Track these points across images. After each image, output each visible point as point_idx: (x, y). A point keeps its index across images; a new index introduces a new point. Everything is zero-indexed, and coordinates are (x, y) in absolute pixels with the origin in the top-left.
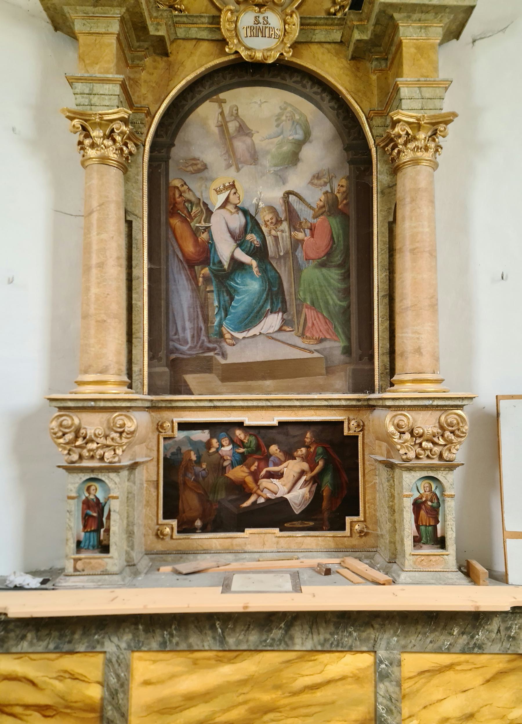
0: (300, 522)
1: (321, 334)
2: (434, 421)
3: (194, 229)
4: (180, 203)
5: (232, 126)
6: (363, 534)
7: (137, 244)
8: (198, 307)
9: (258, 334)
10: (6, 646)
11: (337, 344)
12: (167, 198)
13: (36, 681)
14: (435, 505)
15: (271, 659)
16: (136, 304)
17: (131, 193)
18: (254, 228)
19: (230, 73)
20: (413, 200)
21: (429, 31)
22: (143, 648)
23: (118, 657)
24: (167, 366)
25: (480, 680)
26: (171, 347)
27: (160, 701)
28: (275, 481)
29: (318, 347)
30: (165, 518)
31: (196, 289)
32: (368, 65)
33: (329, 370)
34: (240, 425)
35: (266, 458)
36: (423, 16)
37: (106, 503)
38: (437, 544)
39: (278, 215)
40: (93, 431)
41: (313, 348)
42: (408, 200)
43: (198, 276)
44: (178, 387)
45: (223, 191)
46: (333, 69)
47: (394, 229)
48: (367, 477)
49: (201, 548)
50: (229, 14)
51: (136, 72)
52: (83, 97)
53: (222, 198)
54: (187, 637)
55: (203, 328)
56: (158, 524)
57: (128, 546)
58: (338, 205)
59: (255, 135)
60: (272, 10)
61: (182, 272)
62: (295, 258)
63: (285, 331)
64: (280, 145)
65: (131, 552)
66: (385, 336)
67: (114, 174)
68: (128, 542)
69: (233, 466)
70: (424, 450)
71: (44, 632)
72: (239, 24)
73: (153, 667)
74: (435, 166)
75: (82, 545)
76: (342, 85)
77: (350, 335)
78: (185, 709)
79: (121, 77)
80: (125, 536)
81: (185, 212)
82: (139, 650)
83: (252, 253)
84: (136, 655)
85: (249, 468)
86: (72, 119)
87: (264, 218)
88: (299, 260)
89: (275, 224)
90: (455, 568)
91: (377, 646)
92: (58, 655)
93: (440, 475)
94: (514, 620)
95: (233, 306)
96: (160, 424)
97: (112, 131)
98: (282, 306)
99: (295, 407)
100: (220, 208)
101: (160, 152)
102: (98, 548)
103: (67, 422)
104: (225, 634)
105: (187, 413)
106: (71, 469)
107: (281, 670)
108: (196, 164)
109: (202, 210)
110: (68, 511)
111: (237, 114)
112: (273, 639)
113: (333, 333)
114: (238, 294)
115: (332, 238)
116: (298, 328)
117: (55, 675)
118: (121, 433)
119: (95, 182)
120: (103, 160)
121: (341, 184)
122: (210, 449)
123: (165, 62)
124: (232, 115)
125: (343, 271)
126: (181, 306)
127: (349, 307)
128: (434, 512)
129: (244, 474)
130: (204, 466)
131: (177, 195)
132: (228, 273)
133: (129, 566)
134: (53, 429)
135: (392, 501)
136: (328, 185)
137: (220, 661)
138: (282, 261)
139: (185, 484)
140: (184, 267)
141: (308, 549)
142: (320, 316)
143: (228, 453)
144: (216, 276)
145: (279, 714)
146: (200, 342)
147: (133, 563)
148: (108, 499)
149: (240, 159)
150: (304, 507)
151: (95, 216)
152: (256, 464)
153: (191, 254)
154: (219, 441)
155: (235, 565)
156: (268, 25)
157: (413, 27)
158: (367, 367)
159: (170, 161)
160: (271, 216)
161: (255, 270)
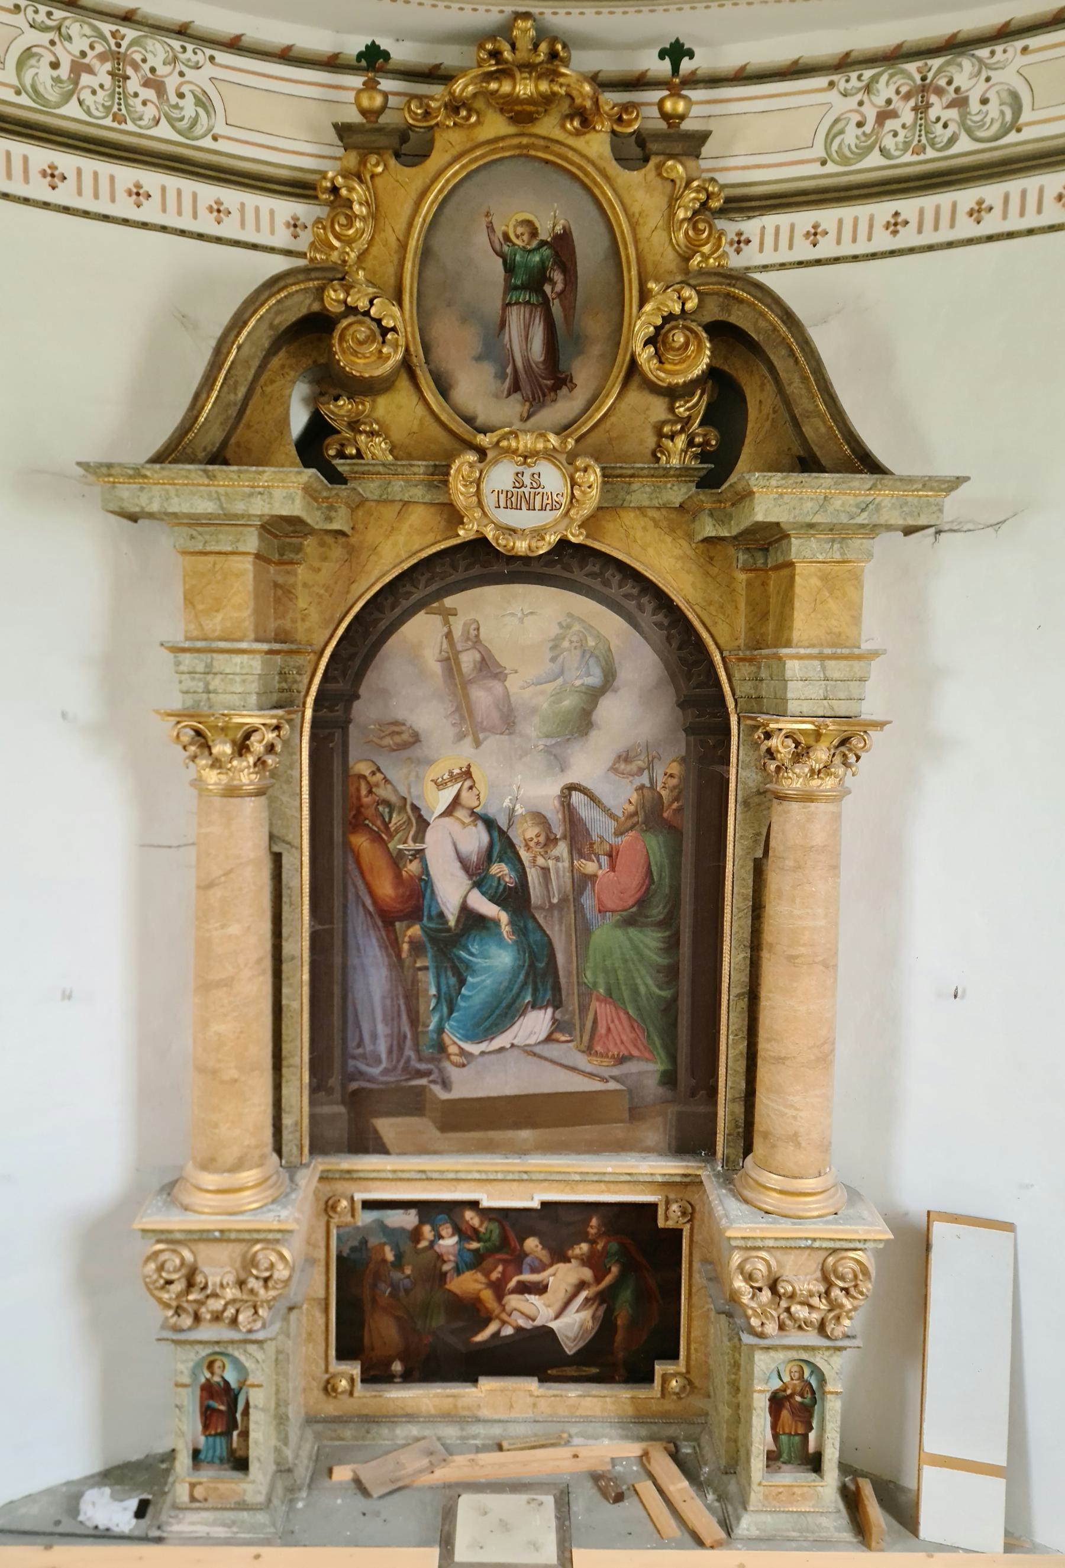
0: (575, 1367)
1: (622, 1048)
2: (814, 1266)
3: (394, 855)
4: (368, 807)
5: (468, 660)
7: (290, 896)
8: (401, 997)
9: (508, 1046)
14: (807, 1401)
16: (288, 1006)
17: (279, 803)
18: (505, 853)
19: (464, 558)
21: (848, 547)
24: (343, 1103)
26: (350, 1069)
28: (533, 1298)
29: (616, 1071)
31: (397, 963)
33: (636, 1114)
34: (474, 1205)
35: (518, 1261)
37: (241, 1389)
38: (807, 1464)
39: (550, 828)
40: (218, 1280)
41: (606, 1072)
42: (790, 863)
43: (400, 940)
44: (364, 1142)
45: (449, 784)
46: (664, 560)
47: (764, 868)
48: (695, 1299)
49: (402, 1412)
50: (466, 468)
51: (288, 572)
52: (193, 679)
53: (446, 796)
55: (409, 1036)
57: (279, 1440)
58: (662, 810)
59: (510, 677)
61: (372, 932)
62: (579, 909)
63: (557, 1041)
64: (558, 696)
65: (284, 1448)
66: (738, 1069)
68: (279, 1432)
69: (458, 1271)
72: (483, 486)
75: (202, 1456)
77: (676, 1050)
81: (379, 823)
85: (487, 1275)
87: (524, 833)
88: (587, 912)
89: (545, 845)
93: (819, 1361)
95: (464, 996)
96: (330, 1202)
98: (554, 995)
100: (443, 815)
101: (332, 711)
102: (229, 1461)
108: (399, 733)
109: (409, 819)
110: (177, 1406)
111: (477, 636)
113: (645, 1047)
115: (649, 872)
116: (581, 1037)
118: (266, 1280)
121: (669, 772)
122: (418, 1242)
123: (343, 547)
124: (468, 639)
125: (667, 934)
126: (369, 992)
127: (675, 999)
131: (364, 792)
132: (457, 934)
133: (281, 1471)
134: (150, 1277)
135: (735, 1374)
136: (646, 772)
138: (556, 913)
139: (374, 1301)
140: (375, 925)
141: (587, 1416)
142: (622, 1015)
143: (451, 1250)
144: (433, 940)
146: (403, 1061)
147: (287, 1467)
149: (482, 723)
150: (582, 1344)
152: (500, 1268)
153: (388, 900)
156: (539, 490)
157: (819, 540)
158: (702, 1109)
159: (352, 728)
160: (536, 830)
161: (505, 929)
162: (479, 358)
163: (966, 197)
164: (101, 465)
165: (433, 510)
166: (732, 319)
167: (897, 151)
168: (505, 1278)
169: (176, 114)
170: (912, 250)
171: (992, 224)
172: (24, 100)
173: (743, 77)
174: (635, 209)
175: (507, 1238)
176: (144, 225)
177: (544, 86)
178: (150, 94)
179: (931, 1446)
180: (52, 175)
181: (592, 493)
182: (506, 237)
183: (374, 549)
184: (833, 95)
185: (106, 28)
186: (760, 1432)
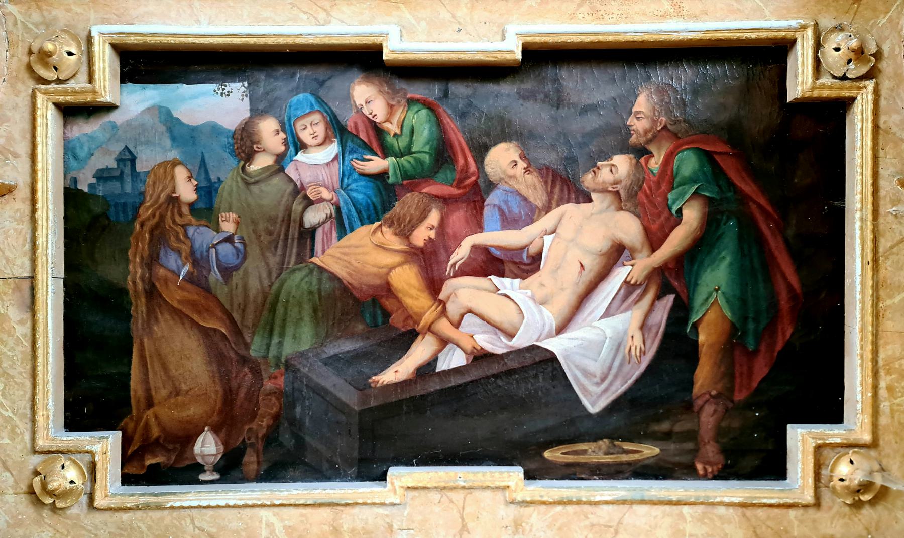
28: (506, 284)
30: (73, 423)
35: (474, 196)
85: (405, 234)
122: (249, 157)
129: (388, 259)
139: (152, 293)
150: (619, 388)
152: (434, 217)
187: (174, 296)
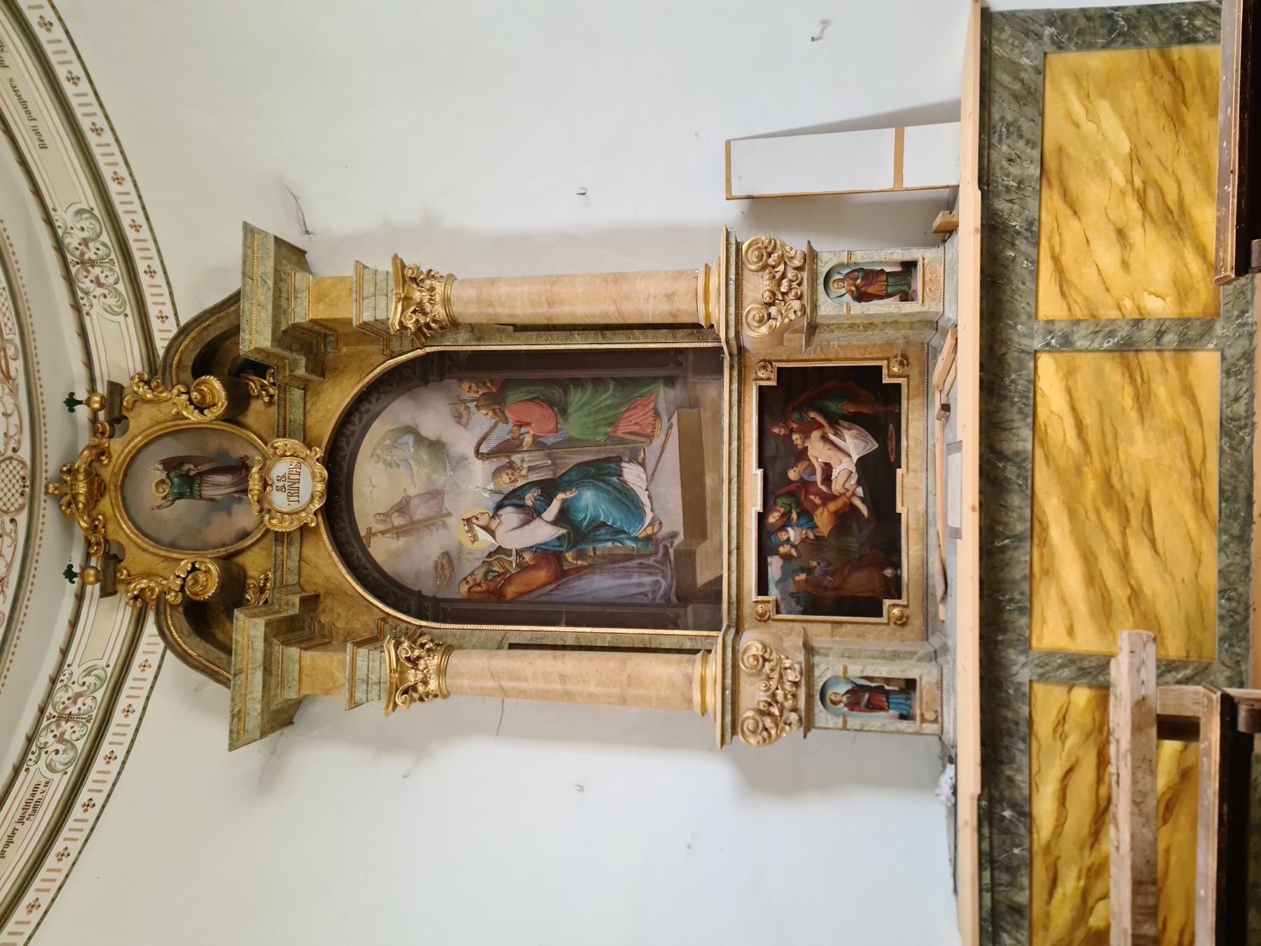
5: (398, 521)
6: (904, 361)
10: (1021, 802)
11: (662, 394)
12: (482, 602)
13: (1067, 768)
14: (860, 275)
15: (1044, 480)
20: (491, 305)
22: (1027, 635)
23: (1037, 665)
24: (685, 607)
25: (1074, 223)
26: (662, 602)
27: (1093, 615)
28: (834, 474)
29: (665, 418)
30: (881, 615)
31: (591, 569)
32: (330, 357)
33: (694, 404)
34: (762, 517)
35: (806, 485)
36: (284, 295)
41: (665, 425)
42: (490, 310)
44: (712, 593)
46: (335, 399)
48: (831, 356)
50: (274, 521)
53: (482, 534)
54: (1014, 582)
56: (888, 624)
60: (270, 470)
62: (556, 446)
64: (420, 463)
67: (457, 661)
68: (905, 658)
70: (790, 289)
71: (1004, 754)
73: (1051, 624)
74: (451, 278)
75: (905, 713)
76: (353, 388)
78: (1105, 585)
79: (349, 646)
80: (898, 662)
82: (1029, 640)
83: (548, 499)
84: (1035, 643)
85: (817, 506)
86: (395, 705)
87: (506, 483)
90: (941, 250)
91: (1028, 349)
92: (1033, 739)
93: (823, 270)
94: (997, 182)
97: (408, 659)
99: (739, 447)
103: (750, 724)
104: (1011, 534)
105: (745, 583)
106: (808, 723)
107: (1058, 467)
112: (1018, 476)
114: (598, 517)
115: (531, 400)
117: (1059, 744)
119: (466, 682)
120: (441, 671)
122: (792, 556)
126: (611, 588)
127: (615, 379)
128: (870, 275)
129: (826, 512)
130: (815, 564)
131: (479, 589)
137: (1045, 542)
139: (836, 589)
140: (565, 583)
145: (1113, 470)
148: (848, 680)
150: (870, 437)
151: (505, 684)
152: (812, 497)
154: (782, 544)
155: (939, 527)
158: (691, 357)
160: (504, 475)
161: (569, 495)
162: (230, 514)
163: (130, 234)
164: (231, 738)
165: (305, 543)
166: (190, 364)
167: (114, 273)
168: (820, 494)
169: (92, 687)
170: (162, 262)
171: (140, 219)
172: (70, 771)
173: (89, 364)
174: (149, 423)
175: (786, 492)
176: (144, 709)
177: (81, 477)
178: (80, 701)
179: (889, 184)
180: (110, 758)
181: (293, 444)
182: (165, 498)
183: (327, 579)
184: (93, 312)
185: (45, 723)
186: (888, 307)
187: (838, 582)
